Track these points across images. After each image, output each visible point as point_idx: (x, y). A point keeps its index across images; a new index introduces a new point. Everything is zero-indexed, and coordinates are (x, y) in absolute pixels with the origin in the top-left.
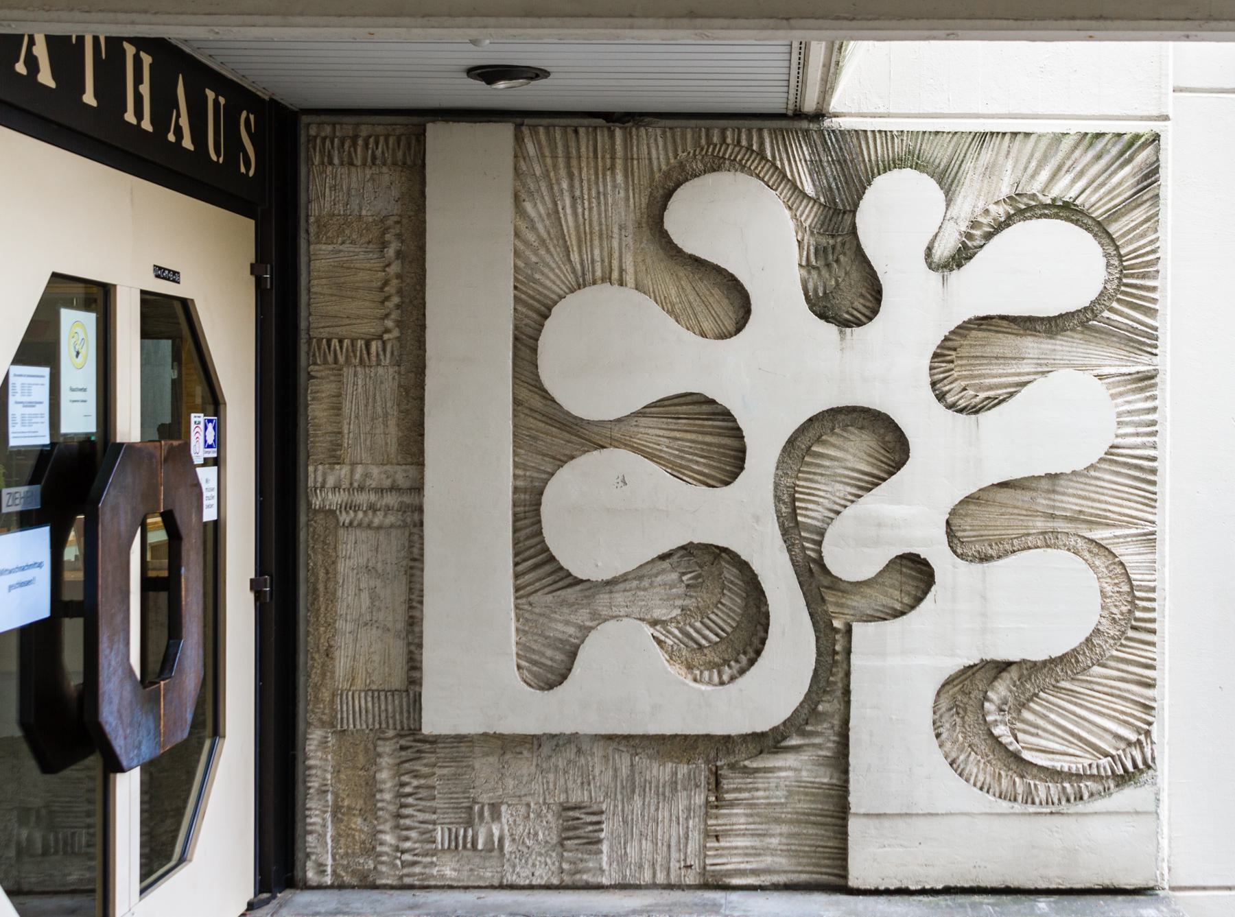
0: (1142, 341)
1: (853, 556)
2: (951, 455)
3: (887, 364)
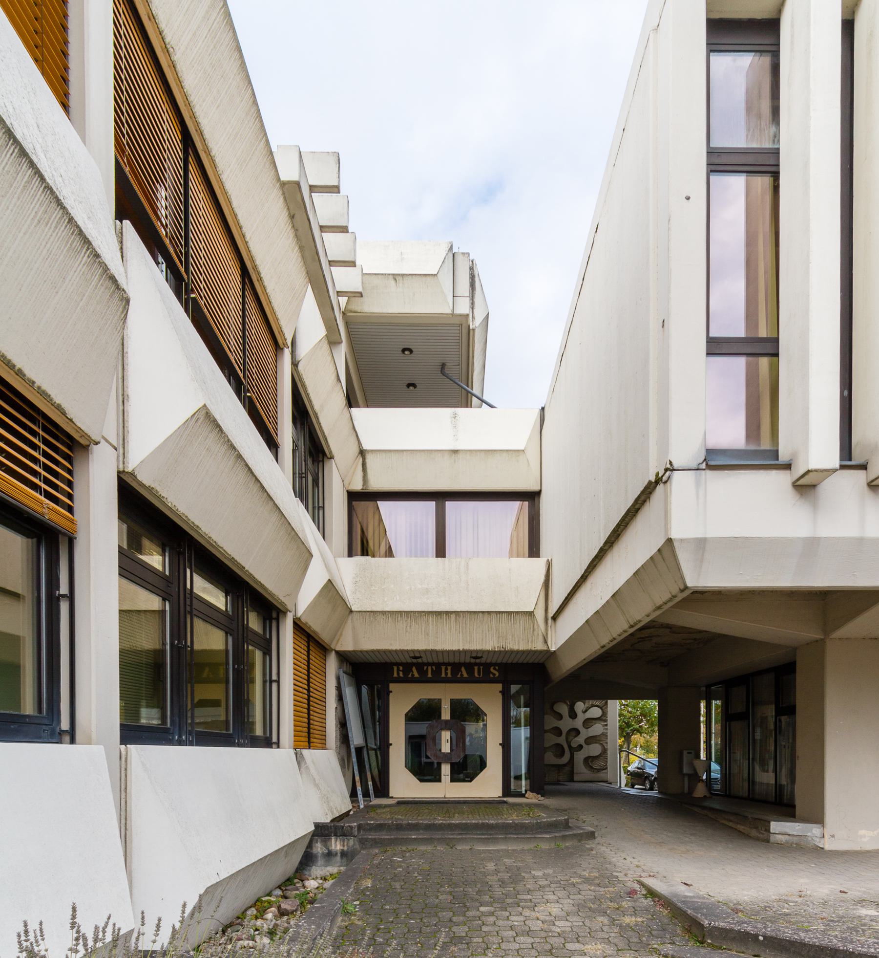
0: (606, 721)
1: (574, 745)
2: (585, 734)
3: (578, 723)
